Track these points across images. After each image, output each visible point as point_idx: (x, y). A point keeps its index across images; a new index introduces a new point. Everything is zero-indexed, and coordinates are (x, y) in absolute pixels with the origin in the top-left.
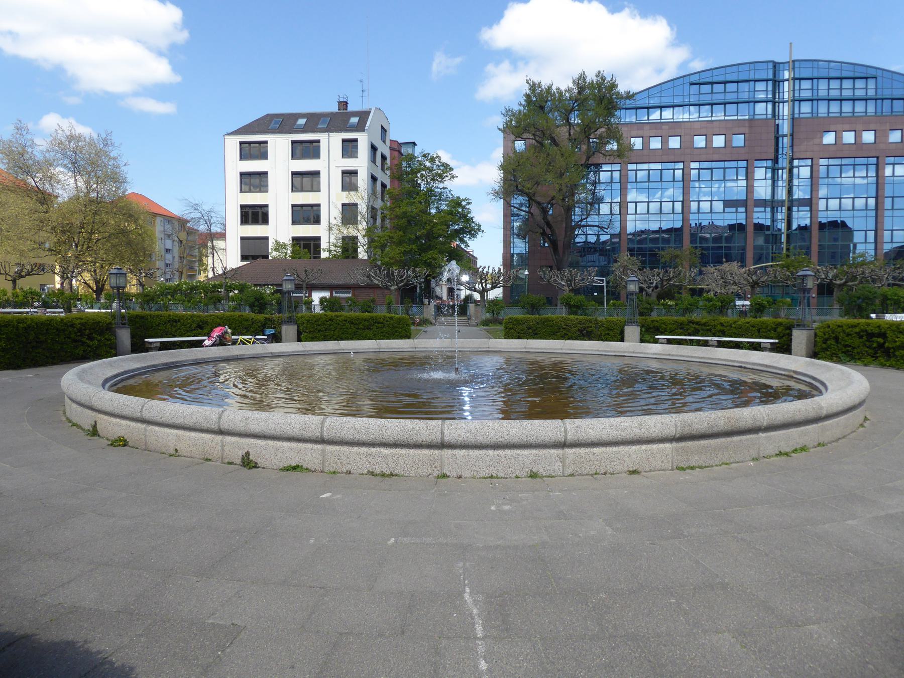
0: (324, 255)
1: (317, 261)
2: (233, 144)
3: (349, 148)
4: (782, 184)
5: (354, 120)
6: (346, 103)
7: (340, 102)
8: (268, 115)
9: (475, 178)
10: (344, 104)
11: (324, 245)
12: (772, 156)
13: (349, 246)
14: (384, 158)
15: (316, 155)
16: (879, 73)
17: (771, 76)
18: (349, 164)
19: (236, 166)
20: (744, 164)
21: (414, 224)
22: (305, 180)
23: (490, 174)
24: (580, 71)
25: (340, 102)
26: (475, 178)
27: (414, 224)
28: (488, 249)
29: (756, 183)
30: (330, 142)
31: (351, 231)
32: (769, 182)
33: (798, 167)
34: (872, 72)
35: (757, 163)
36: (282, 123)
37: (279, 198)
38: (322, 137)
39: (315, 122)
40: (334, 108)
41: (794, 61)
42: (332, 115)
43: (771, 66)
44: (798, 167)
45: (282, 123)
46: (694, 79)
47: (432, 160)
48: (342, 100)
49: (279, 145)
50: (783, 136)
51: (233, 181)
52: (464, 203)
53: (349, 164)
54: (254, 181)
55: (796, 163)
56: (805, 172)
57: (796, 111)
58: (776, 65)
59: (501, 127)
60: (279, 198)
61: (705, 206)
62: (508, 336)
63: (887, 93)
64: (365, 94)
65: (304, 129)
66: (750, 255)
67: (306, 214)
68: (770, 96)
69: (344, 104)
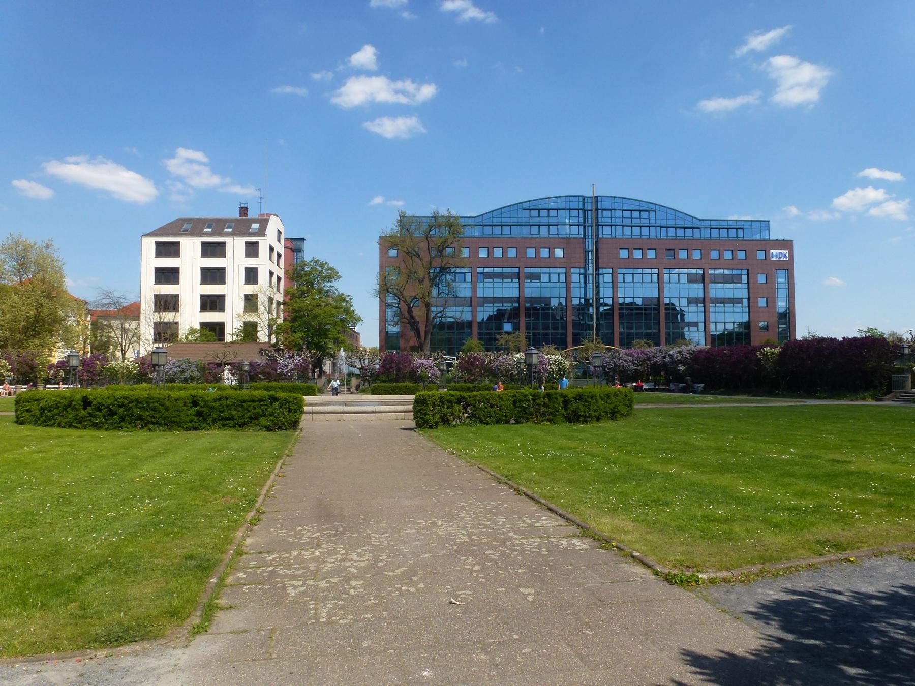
0: (228, 338)
1: (219, 344)
2: (149, 245)
3: (252, 250)
4: (590, 286)
5: (255, 226)
6: (246, 209)
7: (241, 208)
8: (179, 220)
9: (360, 288)
10: (244, 211)
11: (228, 330)
12: (582, 265)
13: (250, 330)
14: (279, 255)
15: (223, 254)
16: (658, 208)
17: (581, 207)
18: (252, 262)
19: (151, 261)
20: (564, 270)
21: (313, 322)
22: (213, 276)
23: (372, 282)
24: (421, 439)
25: (241, 208)
26: (360, 288)
27: (313, 322)
28: (369, 336)
29: (573, 285)
30: (236, 245)
31: (252, 318)
32: (582, 285)
33: (603, 274)
34: (652, 207)
35: (573, 270)
36: (193, 227)
37: (190, 290)
38: (228, 240)
39: (218, 225)
40: (236, 215)
41: (597, 197)
42: (235, 220)
43: (581, 199)
44: (603, 274)
45: (193, 227)
46: (526, 205)
47: (322, 266)
48: (243, 206)
49: (190, 246)
50: (592, 251)
51: (149, 276)
52: (347, 299)
53: (252, 262)
54: (167, 275)
55: (601, 271)
56: (608, 278)
57: (600, 233)
58: (584, 198)
59: (413, 424)
60: (190, 290)
61: (554, 278)
62: (373, 394)
63: (664, 223)
64: (262, 200)
65: (213, 234)
66: (570, 339)
67: (212, 303)
68: (581, 220)
69: (244, 211)
